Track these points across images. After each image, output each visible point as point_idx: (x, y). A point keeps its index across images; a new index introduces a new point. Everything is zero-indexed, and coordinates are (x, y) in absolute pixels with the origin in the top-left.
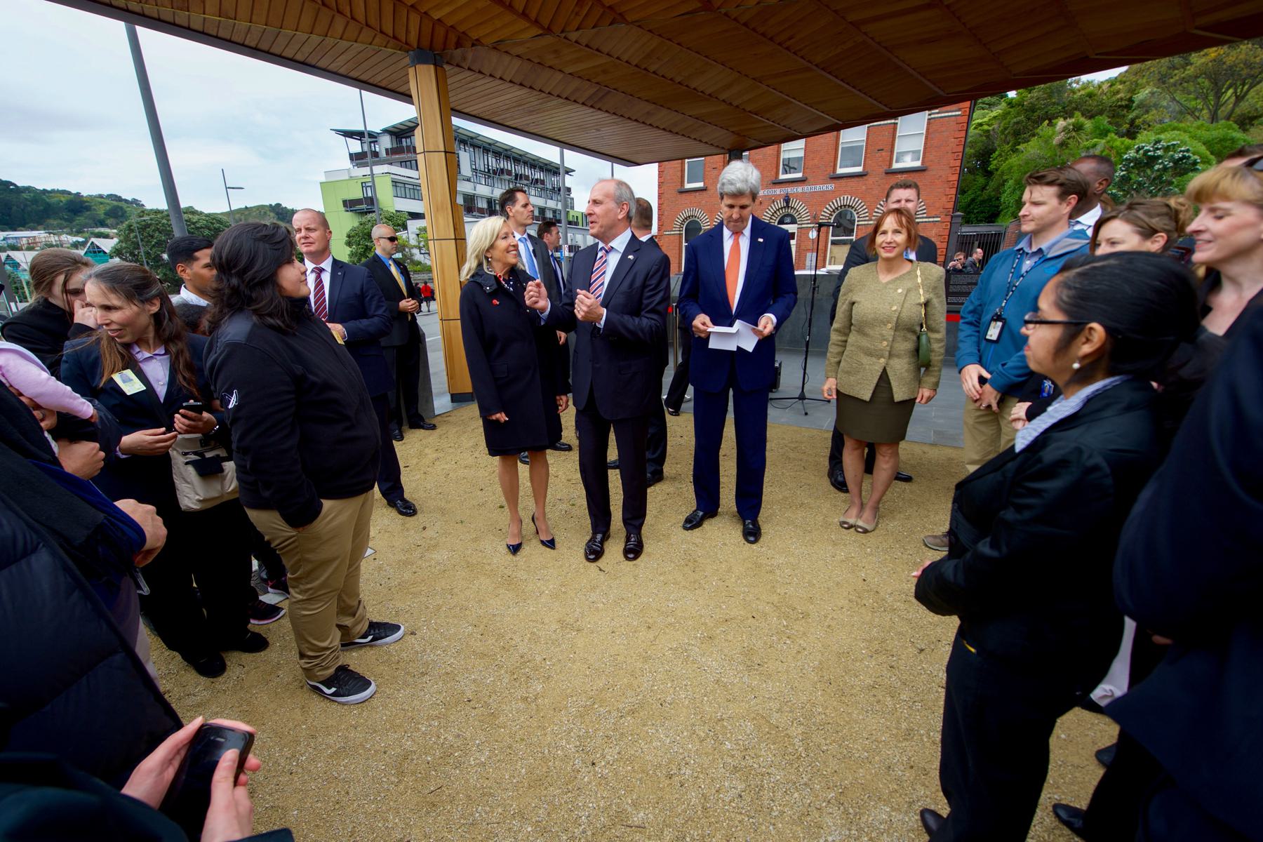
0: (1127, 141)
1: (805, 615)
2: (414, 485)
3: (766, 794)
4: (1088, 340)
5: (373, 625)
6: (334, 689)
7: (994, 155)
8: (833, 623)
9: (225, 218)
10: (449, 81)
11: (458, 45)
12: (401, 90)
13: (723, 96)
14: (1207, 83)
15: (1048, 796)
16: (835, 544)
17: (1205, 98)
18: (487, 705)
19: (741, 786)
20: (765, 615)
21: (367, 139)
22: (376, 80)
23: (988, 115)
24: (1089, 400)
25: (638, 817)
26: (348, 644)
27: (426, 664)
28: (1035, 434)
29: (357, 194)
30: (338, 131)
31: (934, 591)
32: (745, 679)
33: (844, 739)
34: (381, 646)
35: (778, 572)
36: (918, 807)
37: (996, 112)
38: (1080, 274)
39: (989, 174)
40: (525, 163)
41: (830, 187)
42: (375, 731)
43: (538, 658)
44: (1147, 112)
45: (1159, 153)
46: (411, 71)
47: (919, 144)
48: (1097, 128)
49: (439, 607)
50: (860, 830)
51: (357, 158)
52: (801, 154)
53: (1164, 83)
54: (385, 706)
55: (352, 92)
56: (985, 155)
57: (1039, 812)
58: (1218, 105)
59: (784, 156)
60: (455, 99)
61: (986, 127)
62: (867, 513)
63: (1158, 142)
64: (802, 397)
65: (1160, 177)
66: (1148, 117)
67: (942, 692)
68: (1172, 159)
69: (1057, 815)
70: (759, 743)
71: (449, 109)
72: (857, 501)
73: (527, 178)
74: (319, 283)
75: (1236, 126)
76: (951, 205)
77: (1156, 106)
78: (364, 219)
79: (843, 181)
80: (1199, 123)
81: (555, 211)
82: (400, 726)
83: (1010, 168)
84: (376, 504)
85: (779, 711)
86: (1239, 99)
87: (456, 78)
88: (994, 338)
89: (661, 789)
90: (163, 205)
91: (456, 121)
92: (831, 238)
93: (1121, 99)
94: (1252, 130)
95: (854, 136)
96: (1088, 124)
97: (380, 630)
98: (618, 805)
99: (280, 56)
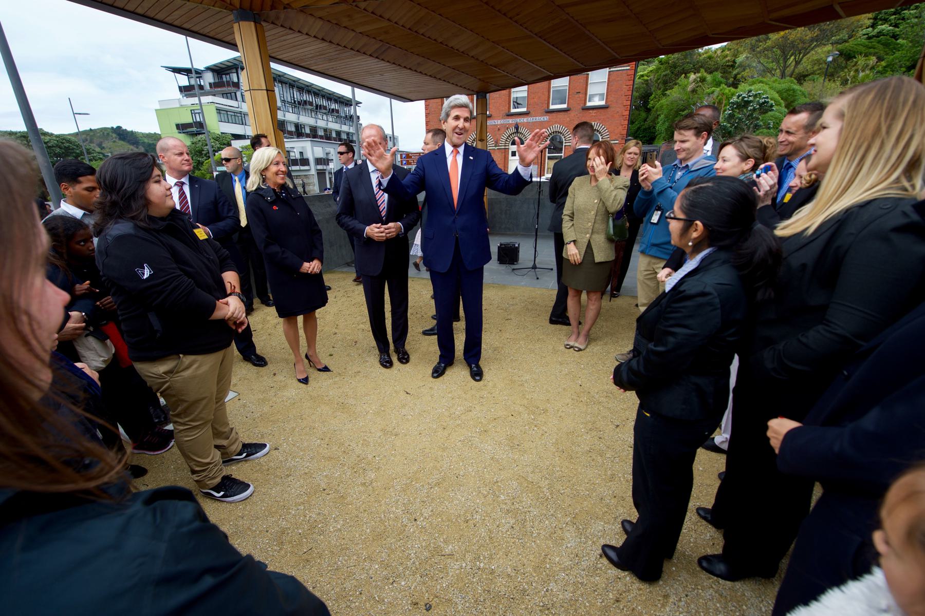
0: (733, 90)
1: (545, 411)
2: (262, 344)
3: (528, 524)
4: (696, 230)
5: (245, 446)
6: (222, 493)
7: (651, 97)
8: (563, 414)
9: (73, 139)
10: (267, 34)
11: (273, 7)
12: (226, 39)
13: (472, 54)
14: (779, 52)
15: (693, 504)
16: (561, 364)
17: (778, 62)
18: (337, 491)
19: (512, 521)
20: (520, 413)
21: (194, 75)
22: (205, 31)
23: (646, 69)
24: (703, 260)
25: (448, 549)
26: (228, 460)
27: (289, 469)
28: (676, 281)
29: (188, 119)
30: (168, 68)
31: (624, 377)
32: (510, 455)
33: (573, 485)
34: (254, 459)
35: (526, 385)
36: (620, 520)
37: (652, 67)
38: (694, 191)
39: (648, 111)
40: (323, 96)
41: (546, 118)
42: (258, 518)
43: (370, 457)
44: (744, 70)
45: (751, 98)
46: (236, 26)
47: (603, 89)
48: (714, 80)
49: (294, 429)
50: (586, 538)
51: (186, 90)
52: (525, 94)
53: (754, 51)
54: (263, 501)
55: (179, 38)
56: (645, 97)
57: (688, 515)
58: (785, 67)
59: (513, 95)
60: (271, 48)
61: (646, 78)
62: (581, 339)
63: (750, 91)
64: (534, 267)
65: (752, 115)
66: (745, 74)
67: (631, 451)
68: (758, 103)
69: (699, 514)
70: (522, 493)
71: (268, 57)
72: (575, 330)
73: (325, 108)
74: (182, 194)
75: (795, 81)
76: (625, 132)
77: (749, 66)
78: (195, 139)
79: (554, 114)
80: (775, 78)
81: (348, 134)
82: (276, 512)
83: (662, 107)
84: (235, 360)
85: (533, 472)
86: (798, 63)
87: (272, 32)
88: (655, 221)
89: (461, 530)
90: (20, 126)
91: (273, 65)
92: (547, 155)
93: (729, 61)
94: (805, 84)
95: (561, 83)
96: (709, 78)
97: (252, 449)
98: (434, 543)
99: (123, 9)
